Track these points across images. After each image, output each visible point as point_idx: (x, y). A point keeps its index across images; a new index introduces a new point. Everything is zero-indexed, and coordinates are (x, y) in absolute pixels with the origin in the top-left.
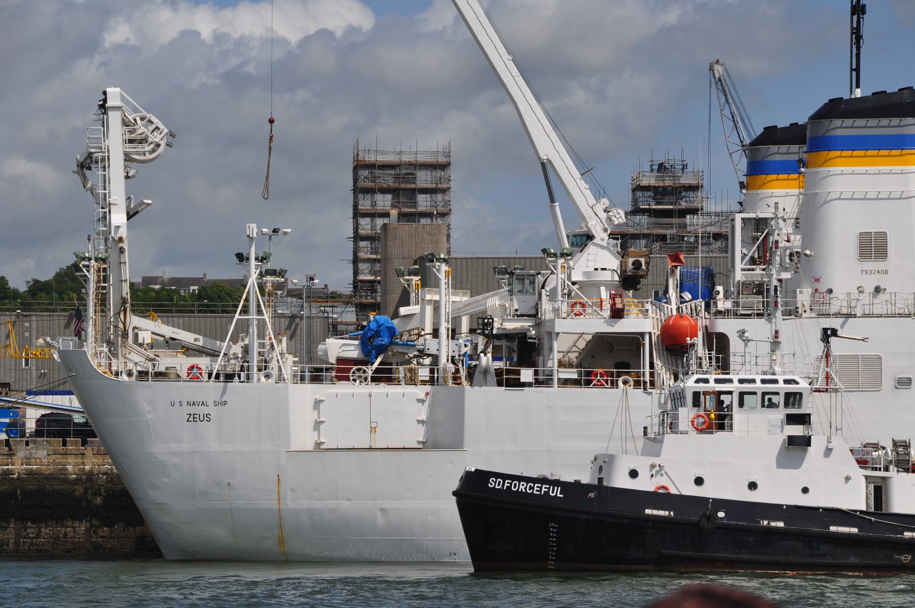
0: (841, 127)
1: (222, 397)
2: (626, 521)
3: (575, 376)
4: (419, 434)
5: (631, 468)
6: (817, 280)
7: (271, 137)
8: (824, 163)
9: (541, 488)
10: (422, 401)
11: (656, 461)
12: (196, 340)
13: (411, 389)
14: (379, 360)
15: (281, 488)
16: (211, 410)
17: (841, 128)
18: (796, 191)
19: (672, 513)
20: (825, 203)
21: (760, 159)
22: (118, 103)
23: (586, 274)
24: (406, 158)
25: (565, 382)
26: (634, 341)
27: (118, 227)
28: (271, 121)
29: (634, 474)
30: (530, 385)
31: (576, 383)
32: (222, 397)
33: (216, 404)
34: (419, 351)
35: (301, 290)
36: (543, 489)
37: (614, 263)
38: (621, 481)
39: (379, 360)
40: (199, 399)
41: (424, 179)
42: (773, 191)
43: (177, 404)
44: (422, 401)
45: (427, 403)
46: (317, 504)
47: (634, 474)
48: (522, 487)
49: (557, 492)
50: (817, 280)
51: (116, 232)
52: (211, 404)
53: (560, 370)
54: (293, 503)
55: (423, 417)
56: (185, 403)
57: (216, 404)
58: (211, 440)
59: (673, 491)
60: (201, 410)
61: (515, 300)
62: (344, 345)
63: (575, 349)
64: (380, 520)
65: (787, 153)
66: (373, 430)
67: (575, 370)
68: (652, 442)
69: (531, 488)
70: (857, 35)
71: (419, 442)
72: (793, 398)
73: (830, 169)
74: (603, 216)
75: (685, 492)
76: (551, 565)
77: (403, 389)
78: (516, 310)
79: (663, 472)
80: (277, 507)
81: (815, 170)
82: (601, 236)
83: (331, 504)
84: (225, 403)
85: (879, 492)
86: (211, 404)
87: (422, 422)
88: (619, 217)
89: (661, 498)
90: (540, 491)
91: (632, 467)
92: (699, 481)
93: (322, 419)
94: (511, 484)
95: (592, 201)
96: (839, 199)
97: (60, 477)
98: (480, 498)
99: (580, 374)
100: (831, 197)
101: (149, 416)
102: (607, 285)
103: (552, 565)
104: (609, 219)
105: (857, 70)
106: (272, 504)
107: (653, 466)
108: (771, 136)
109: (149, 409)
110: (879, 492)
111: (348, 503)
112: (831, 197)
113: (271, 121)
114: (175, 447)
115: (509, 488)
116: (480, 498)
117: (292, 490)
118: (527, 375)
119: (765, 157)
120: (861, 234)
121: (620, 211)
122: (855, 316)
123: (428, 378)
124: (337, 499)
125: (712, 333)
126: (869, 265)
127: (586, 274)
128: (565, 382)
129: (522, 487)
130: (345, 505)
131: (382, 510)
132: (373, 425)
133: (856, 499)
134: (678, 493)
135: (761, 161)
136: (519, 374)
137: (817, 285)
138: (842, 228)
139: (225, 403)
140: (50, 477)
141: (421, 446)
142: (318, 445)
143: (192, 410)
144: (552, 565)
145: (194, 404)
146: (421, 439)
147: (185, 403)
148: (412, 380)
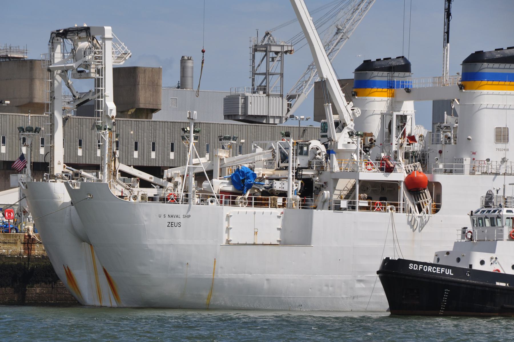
0: (487, 68)
1: (187, 213)
2: (487, 289)
3: (367, 205)
4: (275, 237)
5: (481, 259)
6: (474, 153)
7: (203, 62)
8: (472, 88)
9: (440, 270)
10: (279, 217)
11: (494, 255)
12: (151, 178)
13: (274, 210)
14: (248, 193)
15: (216, 267)
16: (181, 220)
17: (487, 68)
18: (386, 98)
19: (508, 284)
20: (479, 110)
21: (367, 79)
22: (110, 36)
23: (344, 145)
25: (362, 208)
26: (394, 186)
27: (111, 110)
28: (203, 52)
29: (482, 263)
30: (345, 209)
31: (367, 209)
32: (187, 213)
33: (184, 217)
34: (265, 188)
35: (463, 163)
36: (442, 271)
39: (248, 193)
40: (175, 214)
42: (375, 98)
43: (162, 216)
44: (279, 217)
45: (281, 218)
46: (234, 276)
47: (482, 263)
48: (430, 269)
49: (449, 272)
50: (474, 153)
51: (111, 113)
52: (181, 216)
53: (360, 201)
54: (223, 274)
55: (280, 227)
56: (167, 216)
57: (184, 217)
58: (180, 237)
59: (502, 272)
60: (176, 220)
61: (298, 159)
62: (222, 183)
63: (346, 189)
64: (266, 286)
65: (382, 76)
66: (256, 233)
67: (367, 201)
69: (435, 270)
70: (448, 14)
71: (278, 241)
73: (482, 91)
74: (351, 112)
75: (507, 273)
76: (441, 312)
78: (299, 165)
79: (496, 262)
80: (212, 277)
81: (472, 91)
83: (241, 276)
84: (189, 216)
86: (181, 216)
87: (279, 229)
90: (440, 271)
91: (482, 259)
93: (230, 227)
94: (423, 267)
95: (346, 103)
96: (486, 108)
98: (395, 274)
99: (369, 203)
100: (483, 107)
101: (145, 223)
102: (356, 152)
103: (442, 312)
104: (354, 114)
105: (448, 33)
106: (210, 275)
107: (492, 258)
109: (146, 219)
111: (250, 275)
112: (483, 107)
113: (203, 52)
114: (159, 241)
115: (422, 269)
116: (395, 274)
117: (221, 268)
119: (370, 78)
120: (497, 128)
121: (359, 110)
122: (499, 174)
123: (281, 204)
124: (245, 273)
125: (432, 182)
126: (501, 146)
127: (344, 145)
128: (362, 208)
129: (430, 269)
130: (248, 276)
131: (268, 280)
132: (256, 230)
134: (503, 273)
135: (368, 80)
136: (340, 204)
137: (474, 156)
138: (487, 123)
139: (189, 216)
141: (279, 243)
142: (228, 241)
143: (171, 220)
144: (442, 312)
145: (172, 216)
146: (279, 239)
147: (167, 216)
148: (275, 206)
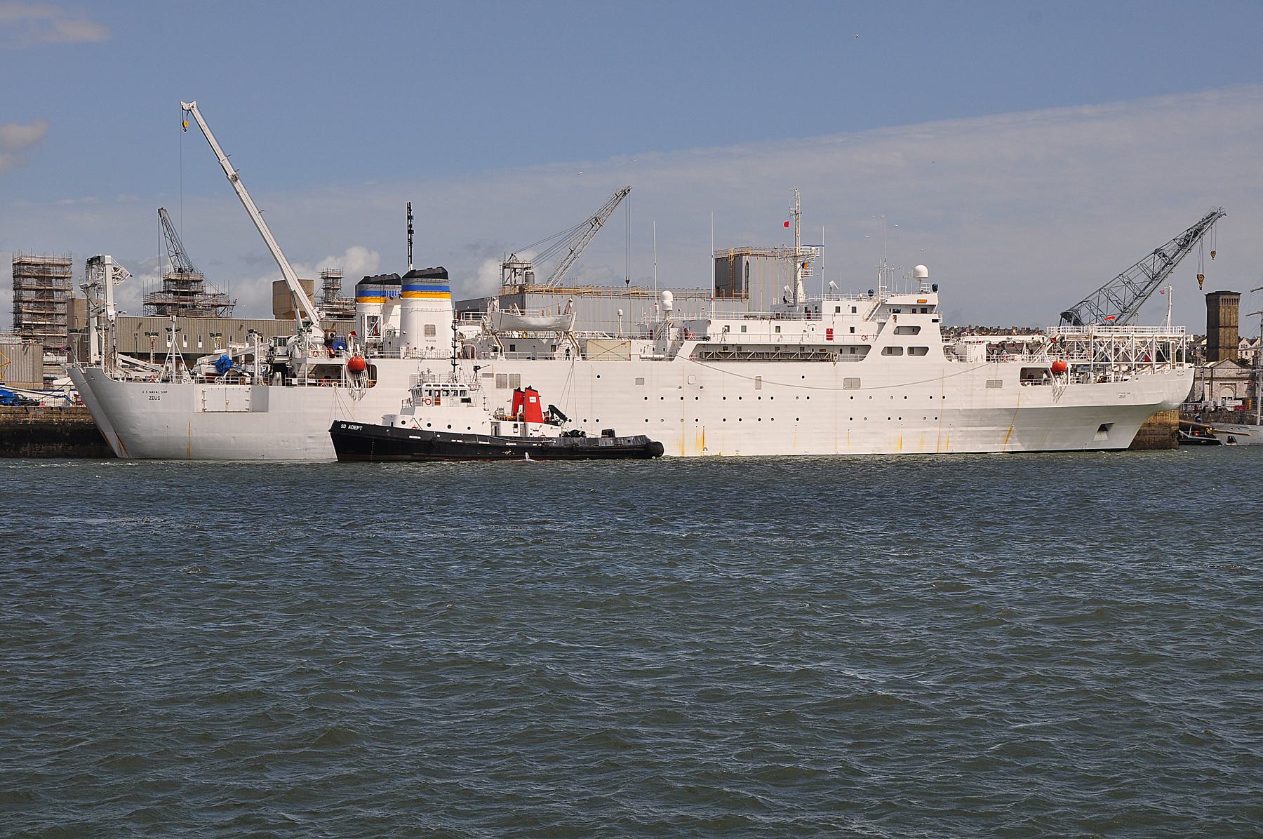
16: (160, 394)
24: (47, 261)
37: (322, 334)
38: (398, 425)
41: (56, 272)
68: (410, 411)
72: (463, 392)
77: (239, 386)
82: (316, 323)
85: (496, 429)
88: (323, 314)
89: (415, 431)
92: (403, 423)
97: (50, 423)
108: (367, 280)
110: (496, 429)
118: (295, 381)
126: (428, 338)
133: (487, 431)
138: (418, 323)
140: (45, 424)
